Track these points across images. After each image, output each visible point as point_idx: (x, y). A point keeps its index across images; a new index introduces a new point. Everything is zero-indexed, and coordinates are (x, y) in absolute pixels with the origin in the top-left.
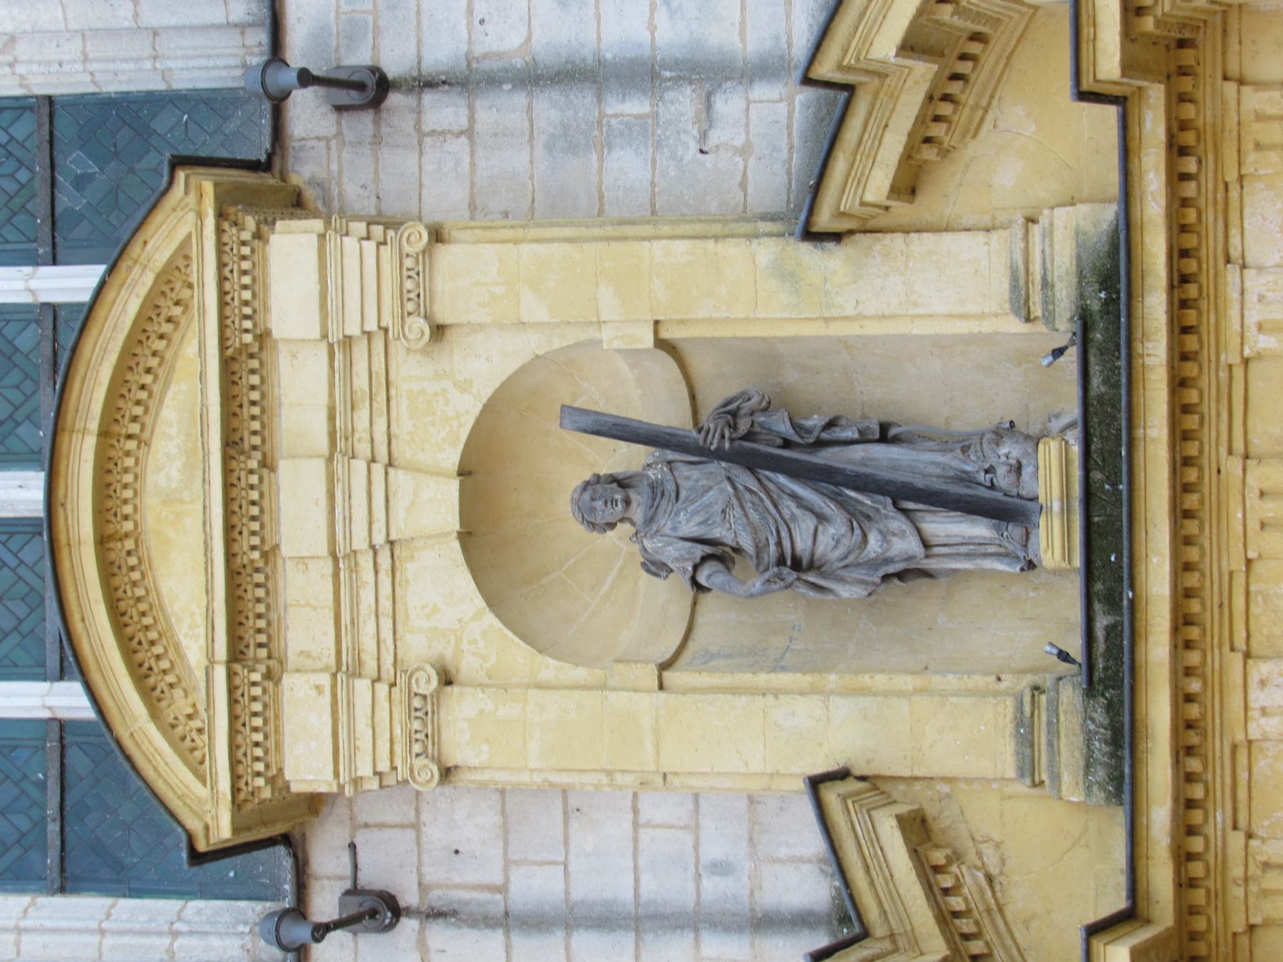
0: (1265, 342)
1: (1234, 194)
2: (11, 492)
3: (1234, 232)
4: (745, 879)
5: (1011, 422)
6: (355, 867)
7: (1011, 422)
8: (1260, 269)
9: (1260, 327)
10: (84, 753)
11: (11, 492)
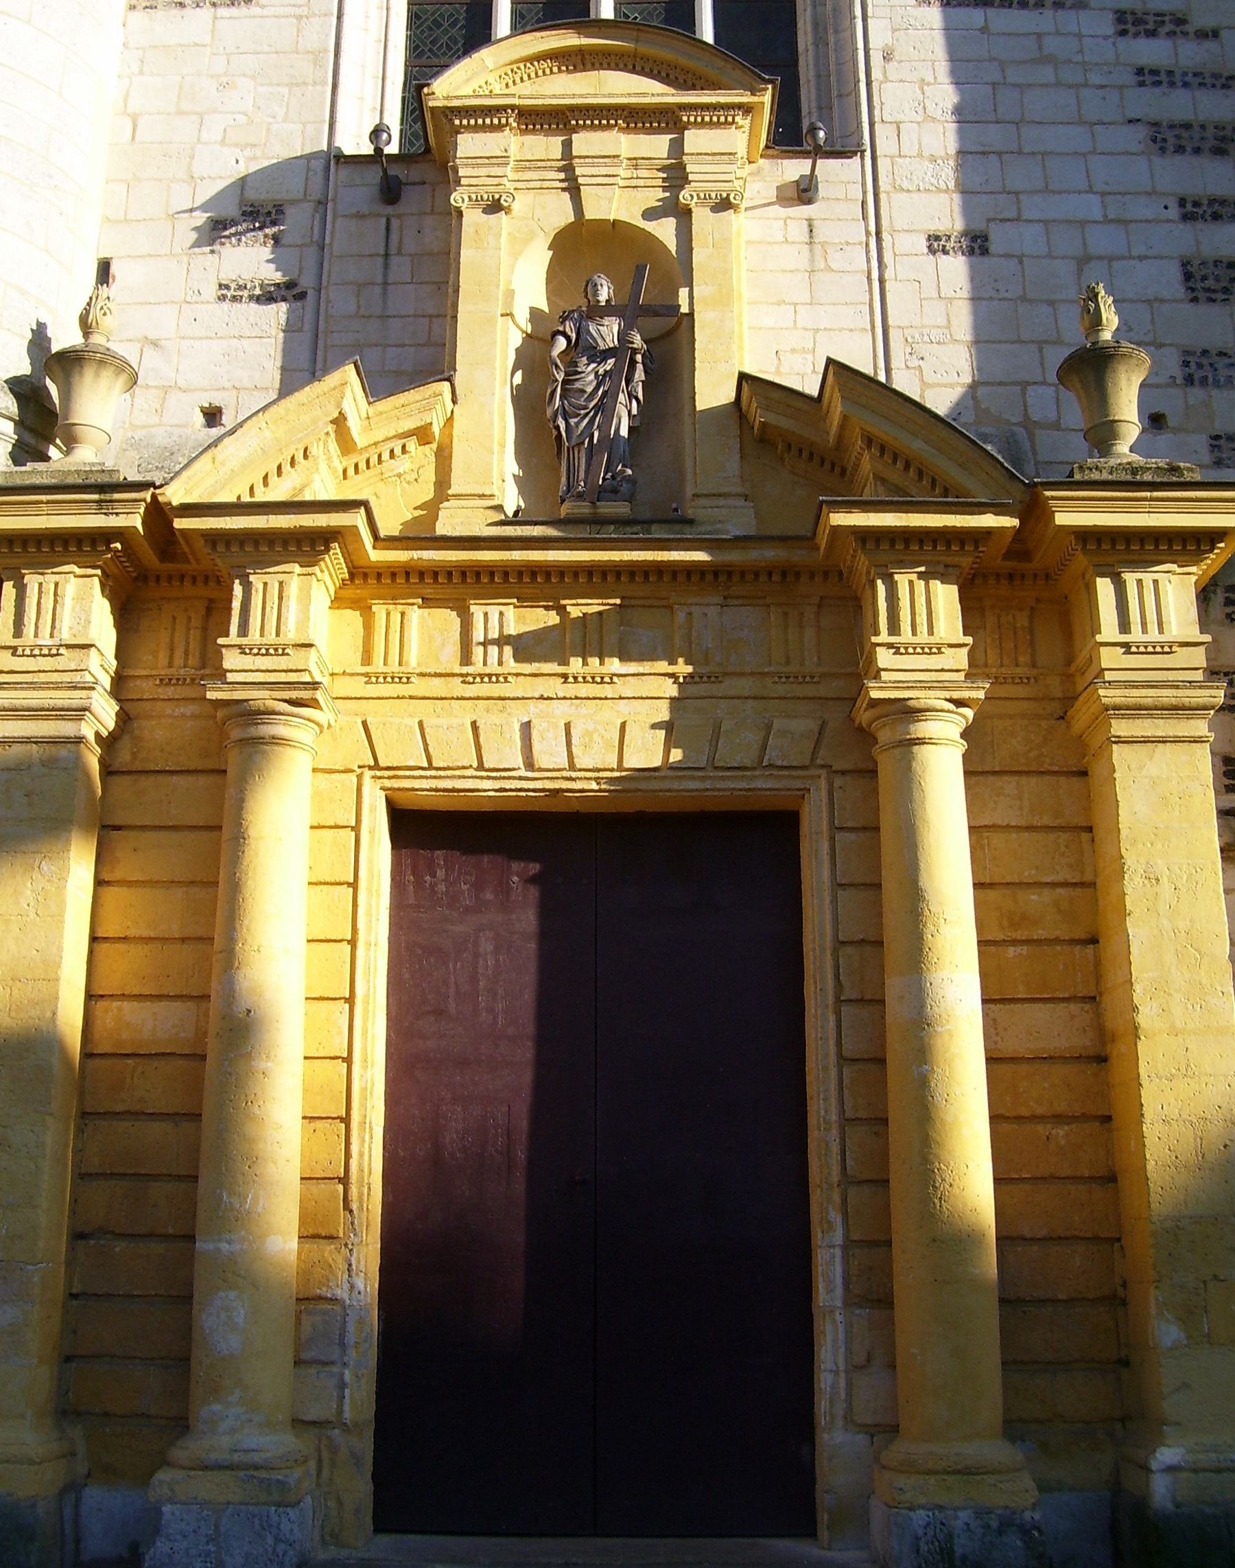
0: (681, 616)
1: (760, 601)
2: (607, 10)
3: (740, 602)
4: (574, 1559)
5: (216, 230)
6: (414, 184)
7: (216, 230)
8: (720, 614)
9: (690, 614)
10: (477, 33)
11: (607, 10)
